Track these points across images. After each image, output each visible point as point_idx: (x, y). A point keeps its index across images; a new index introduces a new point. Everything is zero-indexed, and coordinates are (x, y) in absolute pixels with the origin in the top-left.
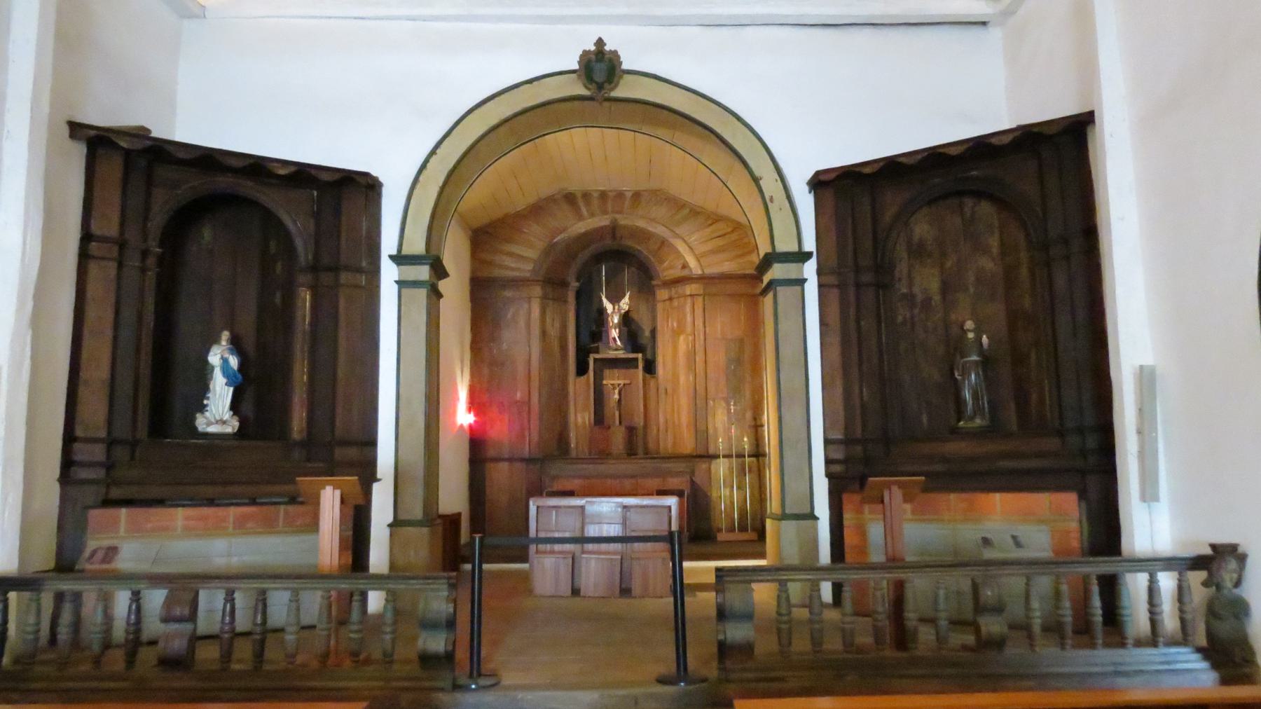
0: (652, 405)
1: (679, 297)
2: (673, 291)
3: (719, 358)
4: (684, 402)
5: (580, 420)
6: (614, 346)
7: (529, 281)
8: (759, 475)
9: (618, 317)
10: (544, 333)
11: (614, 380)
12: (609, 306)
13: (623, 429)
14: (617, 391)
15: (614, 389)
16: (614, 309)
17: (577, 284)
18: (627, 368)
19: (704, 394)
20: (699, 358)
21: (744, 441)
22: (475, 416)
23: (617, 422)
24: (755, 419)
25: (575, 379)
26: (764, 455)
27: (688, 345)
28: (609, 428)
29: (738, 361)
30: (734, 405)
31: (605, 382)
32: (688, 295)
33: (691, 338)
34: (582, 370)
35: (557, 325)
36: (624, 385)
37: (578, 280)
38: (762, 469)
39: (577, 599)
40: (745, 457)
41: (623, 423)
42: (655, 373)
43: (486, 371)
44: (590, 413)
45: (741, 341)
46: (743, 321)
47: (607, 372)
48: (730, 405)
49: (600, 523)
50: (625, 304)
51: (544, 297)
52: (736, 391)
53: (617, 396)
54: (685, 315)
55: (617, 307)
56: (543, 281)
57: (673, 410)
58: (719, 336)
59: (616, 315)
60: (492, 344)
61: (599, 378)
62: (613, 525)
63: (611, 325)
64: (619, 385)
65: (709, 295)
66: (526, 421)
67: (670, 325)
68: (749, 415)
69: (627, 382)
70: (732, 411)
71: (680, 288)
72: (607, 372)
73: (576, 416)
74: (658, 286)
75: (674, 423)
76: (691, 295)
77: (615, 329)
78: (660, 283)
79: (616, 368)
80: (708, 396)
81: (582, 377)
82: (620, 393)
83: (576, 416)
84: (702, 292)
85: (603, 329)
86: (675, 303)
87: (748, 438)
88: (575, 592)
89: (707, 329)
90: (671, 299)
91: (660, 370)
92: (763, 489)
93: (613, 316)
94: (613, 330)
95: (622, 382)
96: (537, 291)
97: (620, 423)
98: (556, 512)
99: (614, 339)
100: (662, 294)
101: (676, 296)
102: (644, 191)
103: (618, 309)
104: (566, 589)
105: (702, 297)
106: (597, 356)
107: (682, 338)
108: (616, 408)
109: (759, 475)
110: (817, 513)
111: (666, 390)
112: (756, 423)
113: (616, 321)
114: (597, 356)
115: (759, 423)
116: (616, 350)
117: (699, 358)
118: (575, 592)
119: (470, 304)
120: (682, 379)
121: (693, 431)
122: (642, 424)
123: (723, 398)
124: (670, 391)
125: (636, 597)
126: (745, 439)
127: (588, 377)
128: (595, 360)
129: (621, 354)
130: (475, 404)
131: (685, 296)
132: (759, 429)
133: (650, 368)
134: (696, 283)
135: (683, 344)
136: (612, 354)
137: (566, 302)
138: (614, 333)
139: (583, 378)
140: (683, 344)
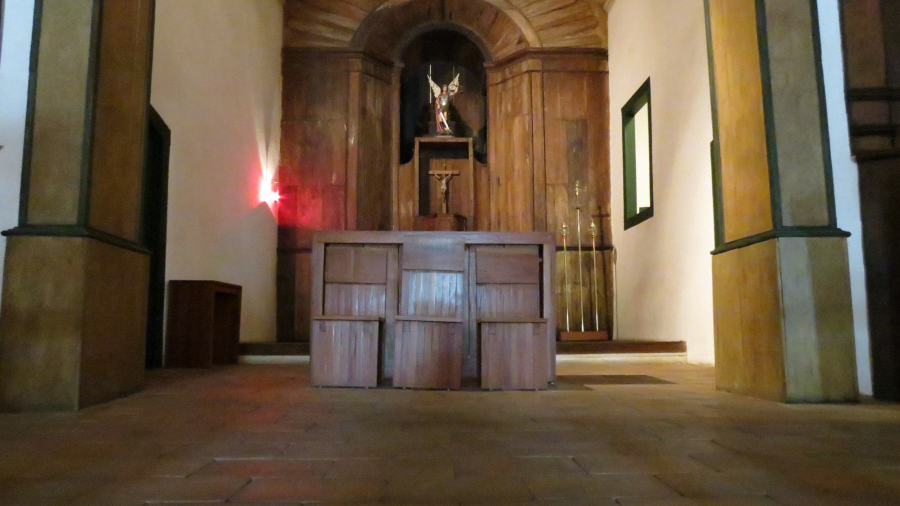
0: (483, 195)
1: (513, 78)
2: (507, 71)
3: (560, 138)
4: (520, 187)
5: (403, 211)
6: (442, 131)
7: (347, 52)
8: (604, 270)
9: (446, 99)
10: (363, 112)
11: (440, 169)
12: (436, 90)
13: (451, 218)
14: (444, 182)
15: (440, 180)
16: (442, 91)
17: (402, 65)
18: (455, 157)
19: (542, 179)
20: (538, 141)
21: (591, 228)
22: (280, 194)
23: (444, 211)
24: (599, 208)
25: (398, 167)
26: (610, 248)
27: (524, 129)
28: (436, 216)
29: (580, 144)
30: (579, 188)
31: (431, 172)
32: (525, 72)
33: (527, 118)
34: (405, 156)
35: (379, 106)
36: (452, 175)
37: (404, 59)
38: (607, 263)
39: (386, 392)
40: (592, 250)
41: (450, 211)
42: (486, 163)
43: (298, 150)
44: (414, 201)
45: (584, 122)
46: (586, 100)
47: (434, 163)
48: (575, 187)
49: (428, 271)
50: (454, 85)
51: (365, 73)
52: (577, 173)
53: (444, 187)
54: (521, 96)
55: (445, 89)
56: (364, 53)
57: (507, 201)
58: (559, 116)
59: (444, 98)
60: (305, 122)
61: (424, 167)
62: (448, 276)
63: (439, 107)
64: (447, 175)
65: (548, 71)
66: (342, 206)
67: (503, 108)
68: (592, 204)
69: (456, 172)
70: (577, 194)
71: (514, 67)
72: (434, 163)
73: (398, 207)
74: (490, 68)
75: (507, 214)
76: (528, 72)
77: (443, 113)
78: (492, 65)
79: (443, 157)
80: (547, 182)
81: (407, 165)
82: (447, 184)
83: (398, 207)
84: (540, 68)
85: (430, 123)
86: (510, 83)
87: (594, 223)
88: (383, 381)
89: (546, 109)
90: (504, 81)
91: (492, 158)
92: (608, 286)
93: (440, 99)
94: (441, 113)
95: (449, 172)
96: (357, 64)
97: (447, 212)
98: (356, 253)
99: (442, 123)
100: (494, 77)
101: (510, 76)
102: (432, 348)
103: (447, 91)
104: (366, 372)
105: (541, 73)
106: (425, 139)
107: (517, 120)
108: (443, 199)
109: (604, 270)
110: (842, 224)
111: (499, 180)
112: (600, 212)
113: (444, 104)
114: (425, 139)
115: (603, 213)
116: (444, 134)
117: (538, 141)
118: (383, 381)
119: (281, 78)
120: (518, 165)
121: (529, 217)
122: (472, 214)
123: (564, 184)
124: (502, 181)
125: (488, 390)
126: (593, 225)
127: (413, 164)
128: (423, 146)
129: (450, 139)
130: (284, 183)
131: (521, 74)
132: (604, 218)
133: (481, 157)
134: (532, 58)
135: (518, 127)
136: (438, 138)
137: (389, 83)
138: (442, 117)
139: (408, 165)
140: (518, 127)
